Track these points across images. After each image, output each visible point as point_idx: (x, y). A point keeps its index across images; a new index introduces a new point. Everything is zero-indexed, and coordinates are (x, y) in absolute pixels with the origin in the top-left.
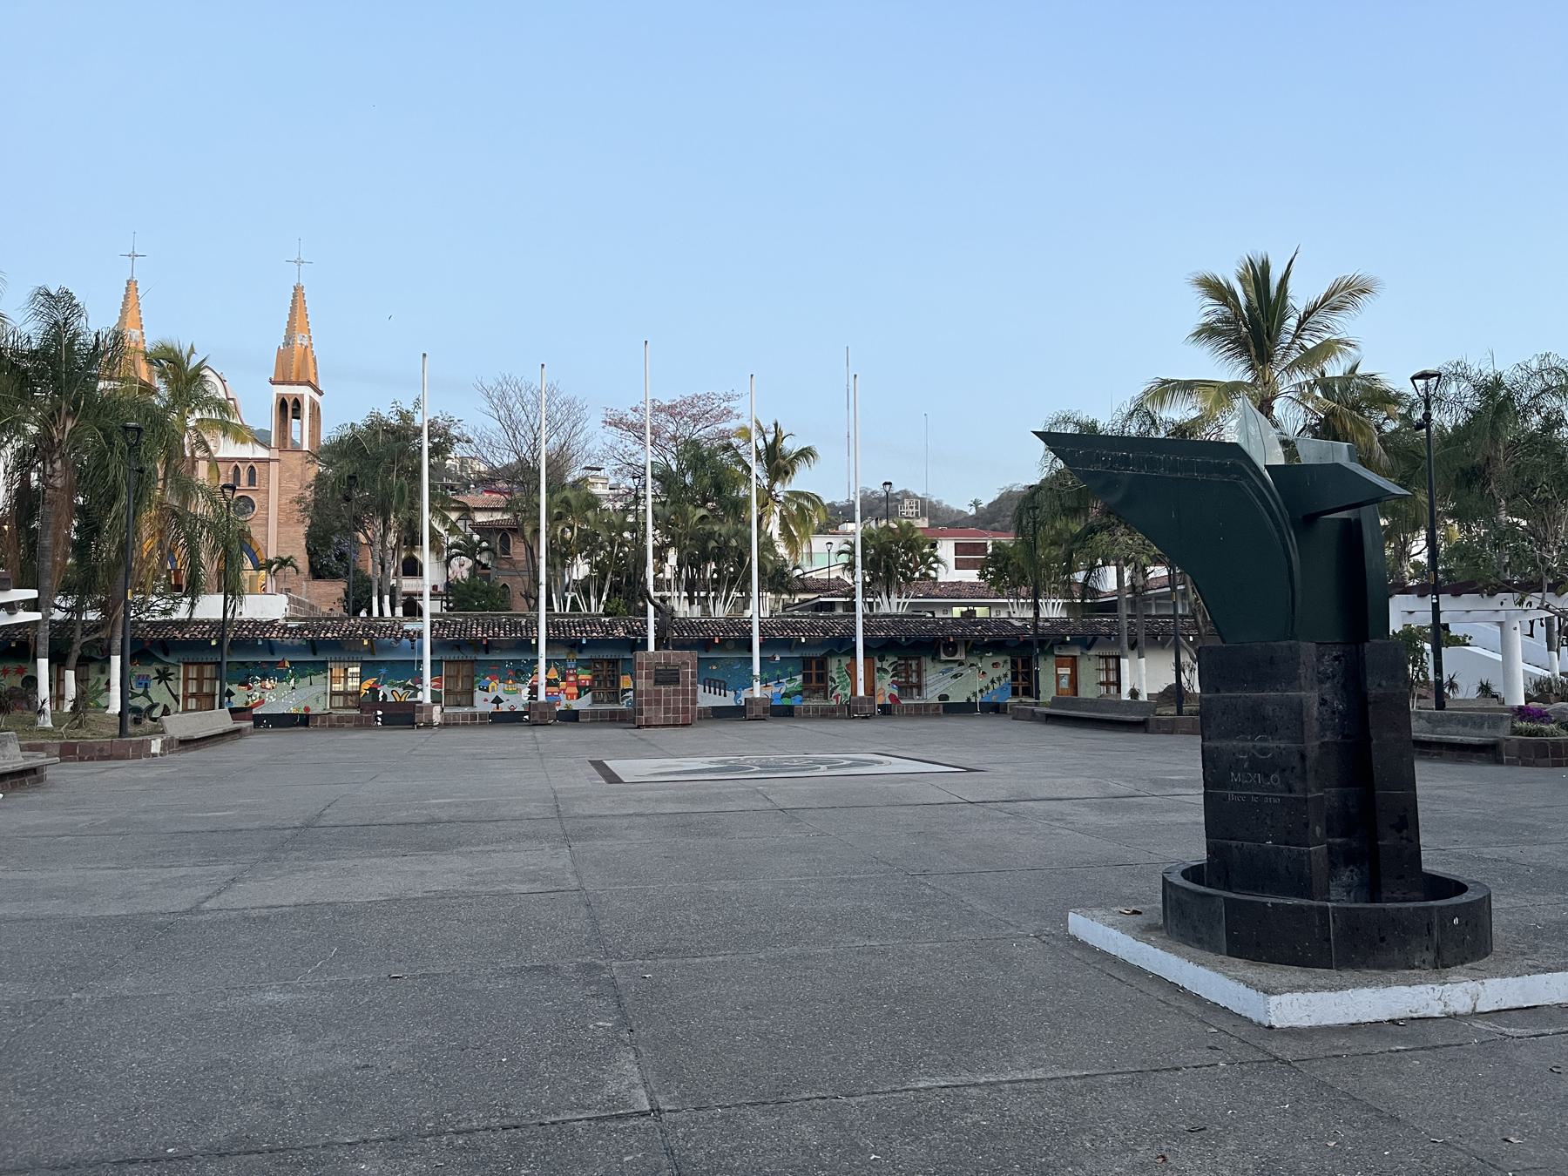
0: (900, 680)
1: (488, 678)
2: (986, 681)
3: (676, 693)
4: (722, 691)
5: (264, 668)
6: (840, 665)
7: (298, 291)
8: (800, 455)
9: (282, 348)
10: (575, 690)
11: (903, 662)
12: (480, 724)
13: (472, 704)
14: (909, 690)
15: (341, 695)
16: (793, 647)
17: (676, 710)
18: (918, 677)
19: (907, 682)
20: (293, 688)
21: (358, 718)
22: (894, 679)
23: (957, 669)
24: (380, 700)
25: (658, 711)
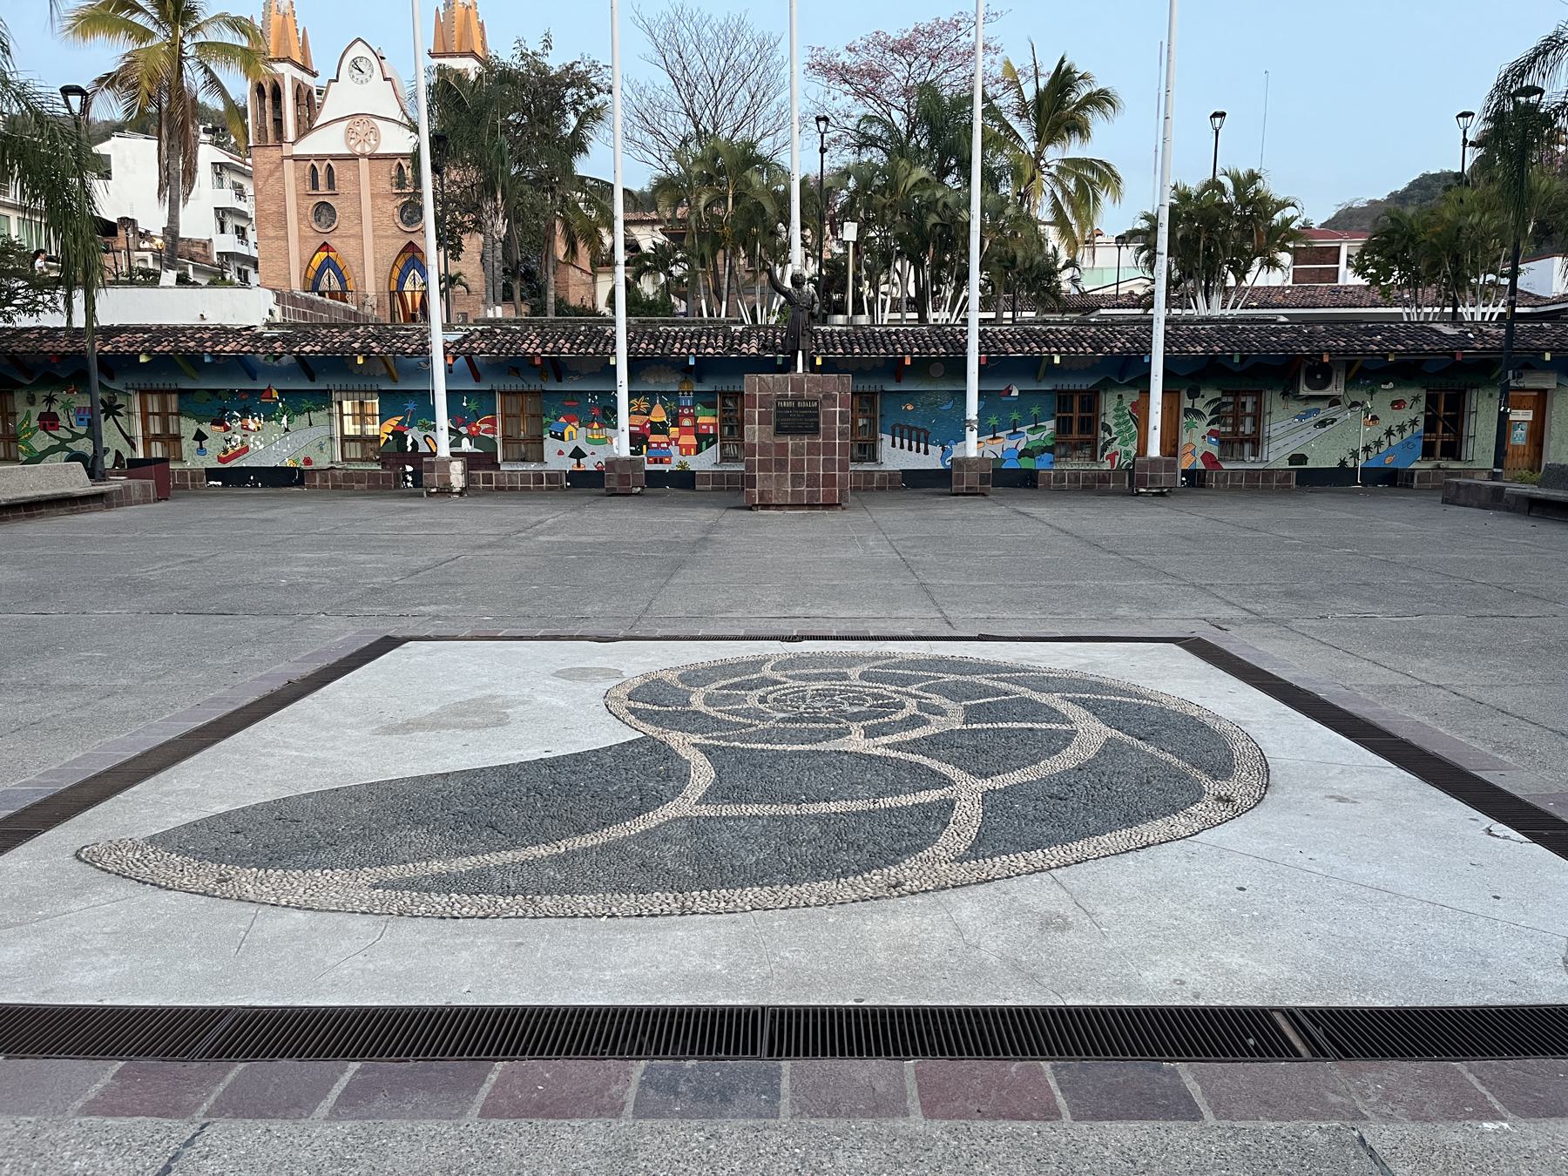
0: (1223, 429)
1: (562, 420)
2: (1378, 432)
3: (812, 449)
4: (922, 446)
5: (243, 400)
6: (1120, 403)
8: (1087, 103)
9: (441, 11)
10: (692, 440)
11: (1231, 399)
12: (549, 489)
13: (541, 460)
14: (1237, 446)
15: (358, 441)
16: (1041, 372)
17: (813, 481)
20: (287, 430)
21: (373, 476)
22: (1212, 427)
23: (1326, 412)
24: (409, 449)
25: (780, 481)
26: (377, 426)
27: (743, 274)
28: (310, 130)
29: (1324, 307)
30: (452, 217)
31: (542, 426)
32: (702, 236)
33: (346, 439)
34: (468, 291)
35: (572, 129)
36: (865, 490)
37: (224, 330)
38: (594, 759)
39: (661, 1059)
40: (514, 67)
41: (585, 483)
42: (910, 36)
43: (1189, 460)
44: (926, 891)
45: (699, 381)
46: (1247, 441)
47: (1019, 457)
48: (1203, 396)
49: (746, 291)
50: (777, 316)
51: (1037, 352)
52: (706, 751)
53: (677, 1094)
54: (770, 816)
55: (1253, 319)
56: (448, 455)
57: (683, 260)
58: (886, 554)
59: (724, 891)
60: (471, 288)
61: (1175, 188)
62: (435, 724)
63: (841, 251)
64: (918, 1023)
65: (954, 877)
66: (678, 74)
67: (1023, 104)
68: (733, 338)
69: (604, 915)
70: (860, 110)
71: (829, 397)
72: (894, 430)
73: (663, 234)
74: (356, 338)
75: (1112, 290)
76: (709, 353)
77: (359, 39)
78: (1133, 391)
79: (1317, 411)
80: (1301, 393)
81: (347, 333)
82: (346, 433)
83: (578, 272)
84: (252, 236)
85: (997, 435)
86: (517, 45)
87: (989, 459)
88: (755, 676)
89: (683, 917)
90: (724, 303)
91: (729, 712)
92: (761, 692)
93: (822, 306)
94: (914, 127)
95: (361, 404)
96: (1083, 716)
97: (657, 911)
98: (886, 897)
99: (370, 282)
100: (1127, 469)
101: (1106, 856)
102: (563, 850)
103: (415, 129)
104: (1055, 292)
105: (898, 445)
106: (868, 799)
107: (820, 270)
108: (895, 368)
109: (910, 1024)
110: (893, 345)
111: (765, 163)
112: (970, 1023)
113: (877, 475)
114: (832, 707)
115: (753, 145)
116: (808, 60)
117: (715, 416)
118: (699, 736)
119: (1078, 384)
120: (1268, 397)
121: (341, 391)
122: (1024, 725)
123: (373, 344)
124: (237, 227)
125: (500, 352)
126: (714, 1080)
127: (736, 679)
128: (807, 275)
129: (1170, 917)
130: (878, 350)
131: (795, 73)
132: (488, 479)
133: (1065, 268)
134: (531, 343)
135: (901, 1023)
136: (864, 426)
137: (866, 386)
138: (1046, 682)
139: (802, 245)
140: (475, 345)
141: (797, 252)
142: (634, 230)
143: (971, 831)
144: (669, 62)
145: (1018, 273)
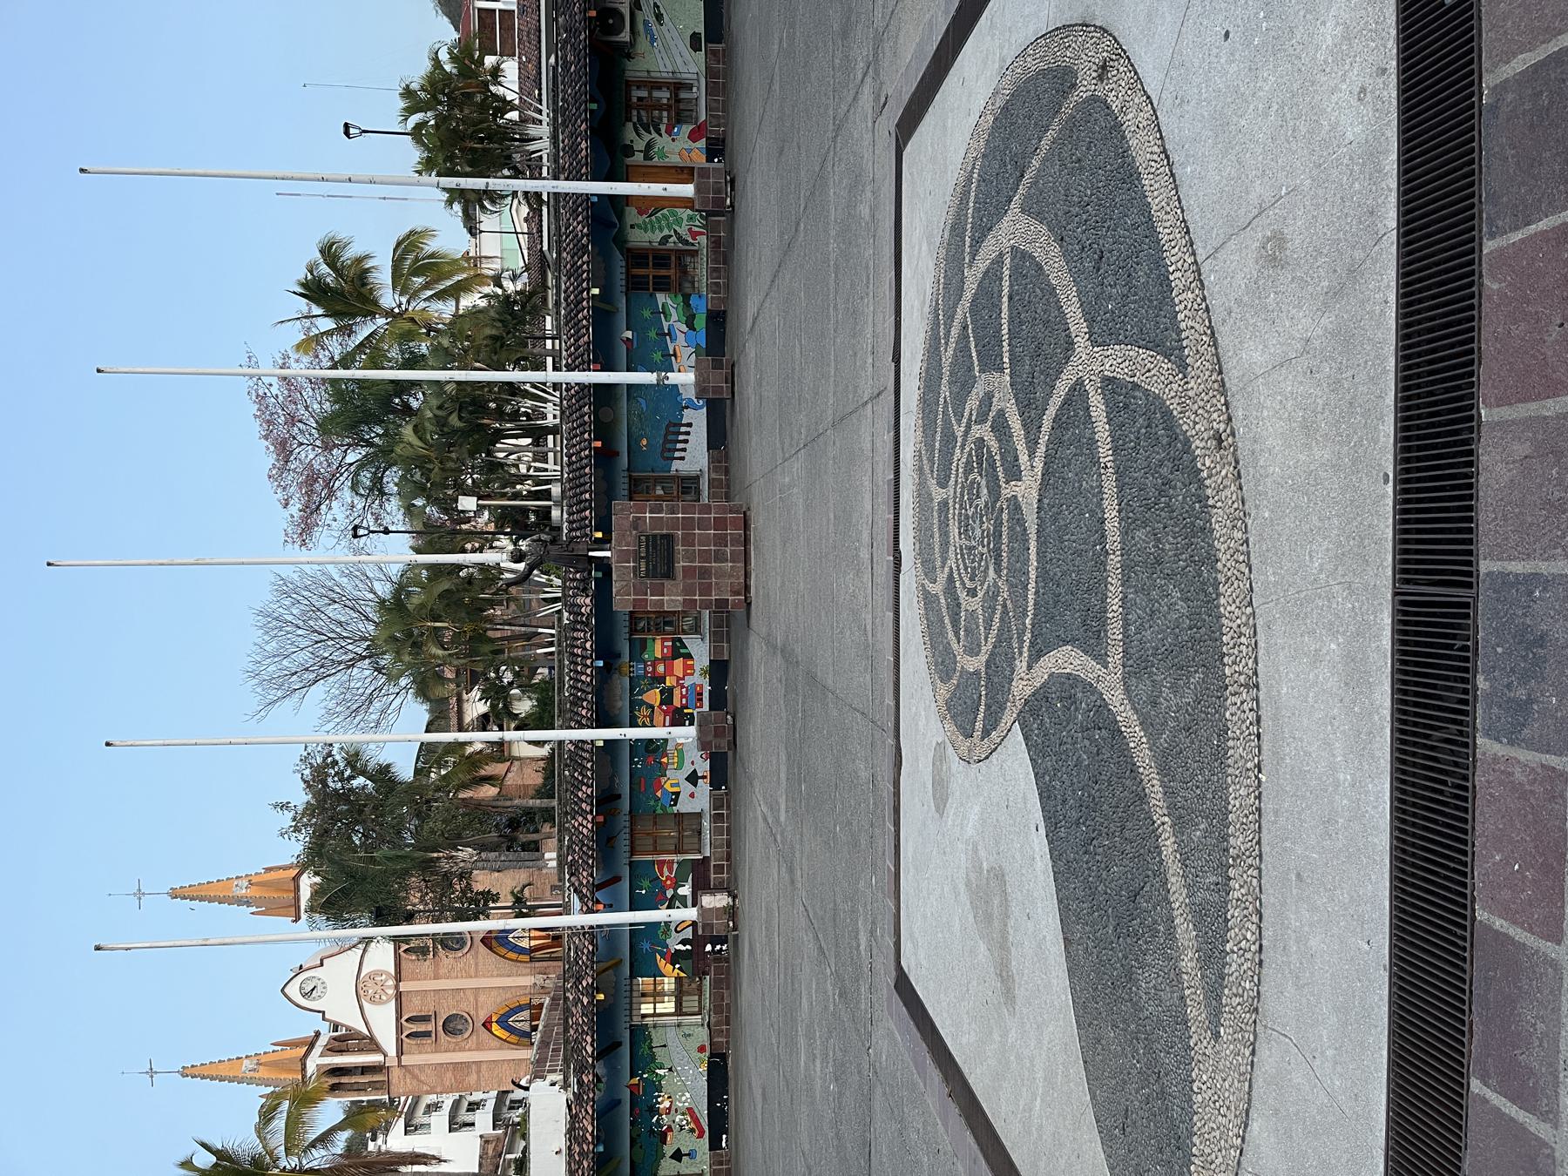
0: (665, 120)
1: (659, 794)
3: (688, 540)
4: (683, 429)
6: (639, 226)
7: (175, 894)
9: (254, 909)
10: (679, 663)
11: (635, 113)
12: (729, 808)
13: (699, 815)
16: (608, 307)
17: (721, 541)
18: (659, 88)
19: (668, 108)
20: (670, 1070)
21: (716, 984)
22: (663, 131)
24: (689, 947)
25: (721, 574)
26: (666, 980)
27: (510, 611)
28: (372, 1039)
29: (539, 21)
30: (456, 902)
31: (666, 814)
32: (473, 653)
33: (679, 1011)
34: (530, 884)
35: (368, 782)
36: (729, 488)
37: (571, 1131)
38: (1047, 778)
39: (1475, 719)
40: (307, 839)
41: (722, 769)
42: (273, 444)
43: (696, 154)
44: (1226, 404)
45: (619, 656)
46: (676, 95)
47: (694, 330)
48: (632, 141)
49: (527, 608)
50: (552, 577)
51: (588, 312)
52: (1037, 655)
53: (1530, 701)
54: (1122, 585)
55: (553, 91)
56: (695, 909)
57: (497, 672)
58: (797, 466)
59: (1224, 638)
60: (527, 882)
61: (419, 173)
62: (1002, 947)
63: (486, 513)
64: (1418, 407)
65: (1208, 373)
66: (312, 676)
67: (339, 329)
68: (576, 622)
69: (1256, 777)
70: (346, 495)
71: (636, 524)
72: (668, 458)
73: (471, 690)
74: (577, 1001)
75: (524, 239)
76: (591, 646)
77: (282, 990)
78: (627, 213)
79: (646, 23)
80: (627, 39)
81: (573, 1009)
82: (673, 1010)
83: (509, 775)
84: (477, 1096)
85: (671, 353)
86: (286, 836)
87: (696, 361)
88: (943, 601)
89: (1261, 686)
90: (540, 630)
91: (988, 628)
92: (963, 595)
93: (542, 531)
94: (363, 440)
95: (644, 995)
96: (993, 241)
97: (1252, 716)
98: (1235, 450)
99: (522, 981)
100: (706, 219)
101: (1179, 200)
102: (1166, 819)
103: (368, 941)
104: (526, 297)
105: (682, 454)
106: (1100, 475)
107: (506, 534)
108: (605, 457)
109: (1419, 417)
110: (582, 459)
111: (400, 589)
112: (1419, 344)
113: (713, 476)
114: (981, 517)
115: (382, 602)
116: (297, 546)
117: (654, 640)
118: (1017, 662)
119: (620, 270)
120: (631, 74)
121: (631, 1016)
122: (1005, 307)
123: (584, 983)
124: (468, 1110)
125: (592, 856)
126: (1510, 655)
127: (947, 620)
128: (511, 547)
129: (1266, 115)
130: (586, 474)
131: (310, 559)
132: (719, 869)
133: (501, 286)
134: (582, 825)
135: (1419, 427)
136: (663, 488)
137: (623, 486)
138: (951, 285)
139: (481, 552)
140: (585, 882)
141: (489, 557)
142: (467, 719)
143: (1144, 356)
144: (302, 685)
145: (508, 333)
